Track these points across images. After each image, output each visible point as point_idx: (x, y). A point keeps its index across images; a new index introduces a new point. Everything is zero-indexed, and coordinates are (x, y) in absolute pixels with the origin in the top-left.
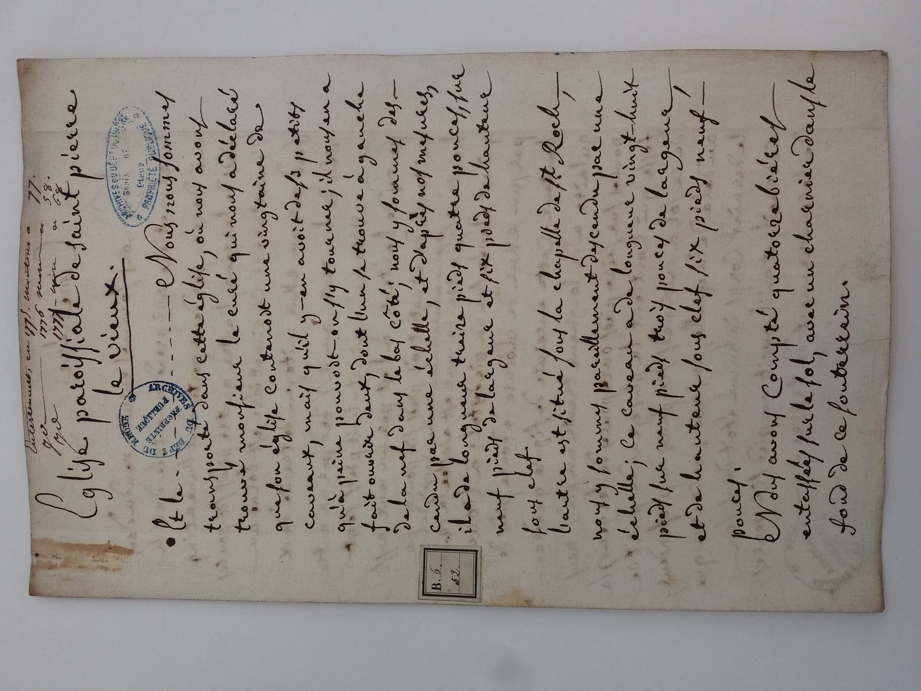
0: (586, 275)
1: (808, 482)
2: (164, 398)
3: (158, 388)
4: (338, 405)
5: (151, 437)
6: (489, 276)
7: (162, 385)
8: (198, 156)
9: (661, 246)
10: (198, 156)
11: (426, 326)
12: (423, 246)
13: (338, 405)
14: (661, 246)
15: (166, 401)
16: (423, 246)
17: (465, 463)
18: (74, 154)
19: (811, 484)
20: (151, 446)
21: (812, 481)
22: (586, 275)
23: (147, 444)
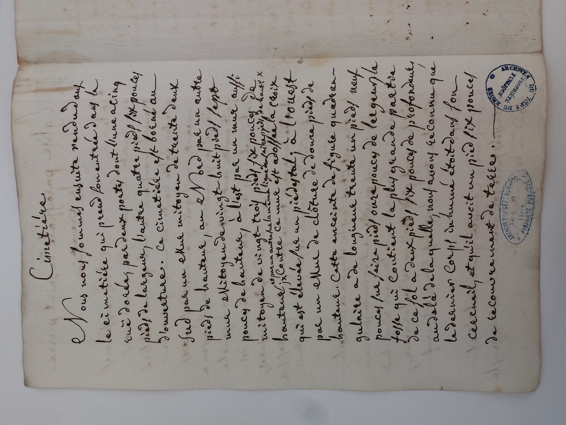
0: (487, 224)
1: (275, 141)
2: (512, 74)
3: (507, 68)
4: (379, 327)
5: (508, 99)
6: (411, 199)
7: (509, 67)
8: (492, 282)
9: (374, 157)
10: (492, 282)
11: (430, 228)
12: (115, 91)
13: (379, 327)
14: (374, 157)
15: (514, 75)
16: (115, 91)
17: (355, 254)
18: (472, 154)
19: (276, 143)
20: (508, 105)
21: (277, 142)
22: (487, 224)
23: (506, 103)
